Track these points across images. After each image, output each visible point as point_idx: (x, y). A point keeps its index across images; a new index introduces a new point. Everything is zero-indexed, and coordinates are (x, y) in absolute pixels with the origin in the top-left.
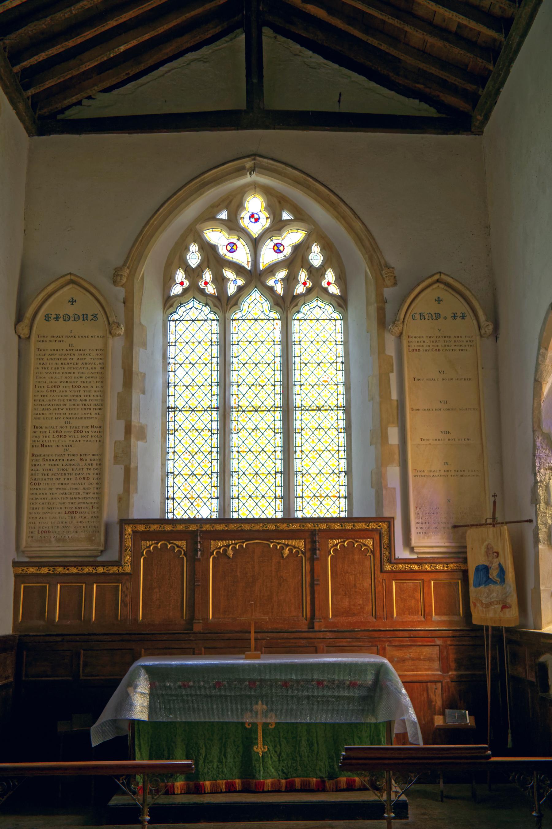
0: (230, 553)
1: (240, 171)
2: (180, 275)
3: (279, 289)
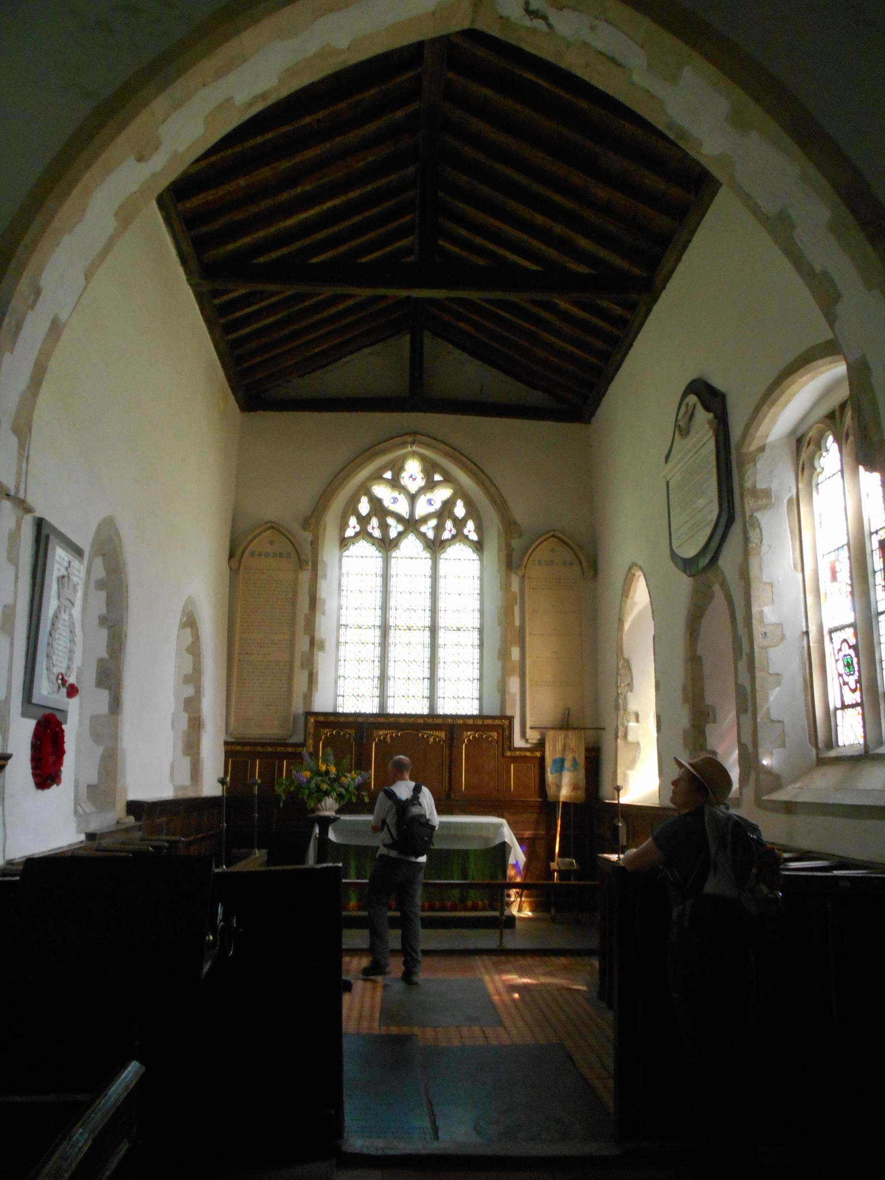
0: (389, 739)
1: (404, 444)
2: (353, 521)
3: (431, 535)
